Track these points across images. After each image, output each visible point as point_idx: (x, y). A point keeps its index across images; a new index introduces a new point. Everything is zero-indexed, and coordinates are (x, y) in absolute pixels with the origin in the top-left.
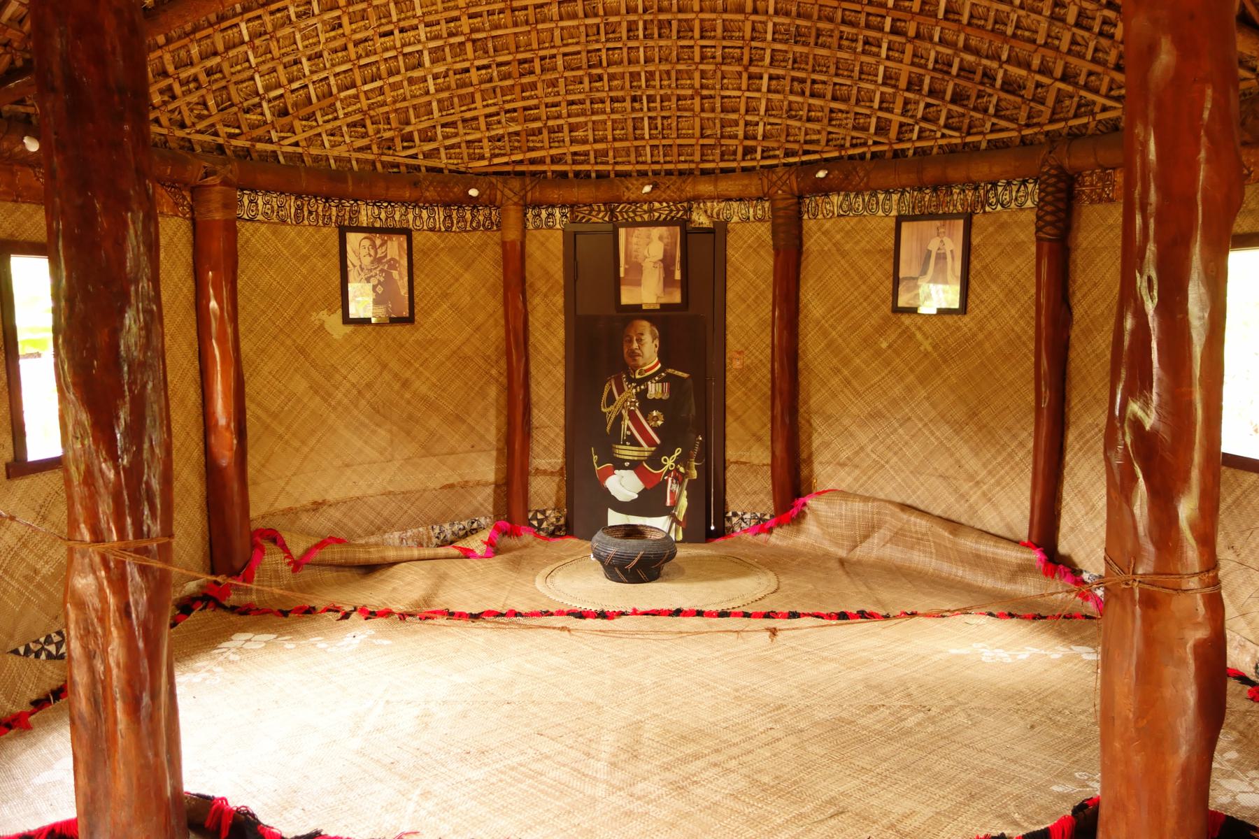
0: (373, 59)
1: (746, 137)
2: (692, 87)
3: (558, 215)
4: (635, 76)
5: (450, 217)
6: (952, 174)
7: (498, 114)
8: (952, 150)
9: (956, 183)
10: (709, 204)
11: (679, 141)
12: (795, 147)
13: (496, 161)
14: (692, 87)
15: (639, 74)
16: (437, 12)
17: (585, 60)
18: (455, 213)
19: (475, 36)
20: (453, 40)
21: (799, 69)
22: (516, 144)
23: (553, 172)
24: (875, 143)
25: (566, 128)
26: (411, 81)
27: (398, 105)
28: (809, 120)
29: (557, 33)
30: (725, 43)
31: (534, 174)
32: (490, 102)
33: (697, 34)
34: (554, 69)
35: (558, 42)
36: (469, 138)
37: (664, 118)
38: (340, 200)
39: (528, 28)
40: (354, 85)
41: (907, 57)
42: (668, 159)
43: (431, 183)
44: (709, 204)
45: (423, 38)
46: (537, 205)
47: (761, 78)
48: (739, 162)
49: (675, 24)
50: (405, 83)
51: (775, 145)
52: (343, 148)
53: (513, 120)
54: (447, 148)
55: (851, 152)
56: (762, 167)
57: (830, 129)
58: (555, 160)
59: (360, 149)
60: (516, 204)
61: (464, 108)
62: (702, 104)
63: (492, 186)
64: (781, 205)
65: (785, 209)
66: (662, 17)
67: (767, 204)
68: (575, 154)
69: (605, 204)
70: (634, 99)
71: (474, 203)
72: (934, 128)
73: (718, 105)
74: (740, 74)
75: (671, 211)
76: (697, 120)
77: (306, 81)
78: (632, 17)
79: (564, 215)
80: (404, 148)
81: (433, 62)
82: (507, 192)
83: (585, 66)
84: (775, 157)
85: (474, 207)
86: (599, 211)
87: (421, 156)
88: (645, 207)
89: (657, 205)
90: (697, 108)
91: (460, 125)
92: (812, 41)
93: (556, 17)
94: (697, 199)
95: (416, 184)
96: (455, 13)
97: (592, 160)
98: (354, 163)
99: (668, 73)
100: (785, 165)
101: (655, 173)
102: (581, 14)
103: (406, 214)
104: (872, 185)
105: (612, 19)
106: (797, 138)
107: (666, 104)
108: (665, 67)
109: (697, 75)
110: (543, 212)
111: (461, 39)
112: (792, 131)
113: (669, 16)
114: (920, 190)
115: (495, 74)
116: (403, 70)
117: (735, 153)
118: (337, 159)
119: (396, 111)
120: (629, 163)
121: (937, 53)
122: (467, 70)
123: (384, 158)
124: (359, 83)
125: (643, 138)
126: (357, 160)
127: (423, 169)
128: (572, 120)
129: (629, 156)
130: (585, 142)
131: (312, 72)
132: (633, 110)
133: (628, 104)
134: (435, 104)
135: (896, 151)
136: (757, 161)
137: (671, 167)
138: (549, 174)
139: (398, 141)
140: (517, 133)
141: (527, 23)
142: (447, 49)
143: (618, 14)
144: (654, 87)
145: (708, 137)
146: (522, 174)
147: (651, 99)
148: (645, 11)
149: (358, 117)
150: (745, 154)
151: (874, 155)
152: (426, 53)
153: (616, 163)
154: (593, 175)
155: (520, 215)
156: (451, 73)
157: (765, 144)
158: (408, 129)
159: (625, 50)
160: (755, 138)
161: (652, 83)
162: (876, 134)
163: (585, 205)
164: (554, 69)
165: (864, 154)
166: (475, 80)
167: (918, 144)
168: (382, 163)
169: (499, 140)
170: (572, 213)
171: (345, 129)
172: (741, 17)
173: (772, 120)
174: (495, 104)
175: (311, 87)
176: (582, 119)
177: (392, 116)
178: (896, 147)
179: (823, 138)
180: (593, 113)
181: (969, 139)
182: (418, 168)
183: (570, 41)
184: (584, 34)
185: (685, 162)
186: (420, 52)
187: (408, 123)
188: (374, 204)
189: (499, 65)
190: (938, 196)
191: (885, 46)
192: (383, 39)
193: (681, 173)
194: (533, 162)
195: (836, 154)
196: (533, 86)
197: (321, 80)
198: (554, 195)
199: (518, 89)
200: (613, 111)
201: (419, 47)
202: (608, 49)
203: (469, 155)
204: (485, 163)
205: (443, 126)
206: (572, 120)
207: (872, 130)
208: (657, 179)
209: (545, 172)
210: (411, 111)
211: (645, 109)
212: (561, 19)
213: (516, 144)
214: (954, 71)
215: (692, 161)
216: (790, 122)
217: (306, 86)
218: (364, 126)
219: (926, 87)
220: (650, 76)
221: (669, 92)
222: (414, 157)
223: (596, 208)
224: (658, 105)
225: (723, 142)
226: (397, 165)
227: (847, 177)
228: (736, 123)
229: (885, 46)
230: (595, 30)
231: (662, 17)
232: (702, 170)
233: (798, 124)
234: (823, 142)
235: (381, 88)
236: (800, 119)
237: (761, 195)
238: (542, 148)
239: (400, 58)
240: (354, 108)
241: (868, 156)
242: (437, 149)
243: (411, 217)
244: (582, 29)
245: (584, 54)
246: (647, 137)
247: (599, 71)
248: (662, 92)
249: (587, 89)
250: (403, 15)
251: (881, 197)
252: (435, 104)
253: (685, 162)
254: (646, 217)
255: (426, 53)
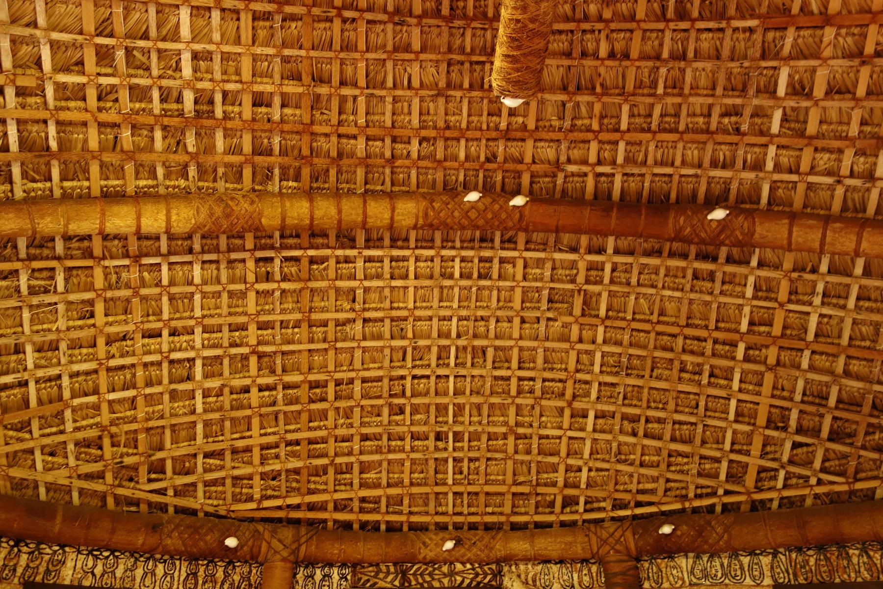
0: (128, 361)
1: (566, 485)
2: (506, 423)
3: (336, 577)
4: (441, 409)
5: (195, 575)
6: (849, 528)
7: (277, 446)
8: (834, 499)
9: (853, 540)
10: (522, 567)
11: (487, 488)
12: (627, 497)
13: (266, 504)
14: (506, 423)
15: (446, 408)
16: (220, 315)
17: (386, 388)
18: (202, 569)
19: (261, 349)
20: (234, 351)
21: (630, 405)
22: (294, 485)
23: (335, 521)
24: (727, 493)
25: (356, 468)
26: (174, 395)
27: (151, 424)
28: (642, 465)
29: (358, 354)
30: (547, 375)
31: (311, 523)
32: (269, 430)
33: (515, 364)
34: (350, 397)
35: (357, 364)
36: (236, 472)
37: (471, 460)
38: (38, 544)
39: (325, 346)
40: (96, 392)
41: (767, 389)
42: (473, 510)
43: (177, 527)
44: (522, 567)
45: (198, 344)
46: (311, 563)
47: (585, 416)
48: (558, 515)
49: (490, 353)
50: (166, 397)
51: (601, 494)
52: (64, 472)
53: (294, 455)
54: (207, 484)
55: (697, 503)
56: (584, 521)
57: (670, 476)
58: (339, 506)
59: (89, 477)
60: (284, 560)
61: (235, 436)
62: (516, 445)
63: (257, 536)
64: (616, 568)
65: (623, 573)
66: (478, 343)
67: (594, 568)
68: (363, 500)
69: (395, 564)
70: (438, 437)
71: (230, 557)
72: (808, 473)
73: (535, 446)
74: (561, 411)
75: (477, 575)
76: (510, 463)
77: (26, 376)
78: (444, 342)
79: (343, 577)
80: (150, 481)
81: (206, 376)
82: (275, 543)
83: (386, 395)
84: (599, 509)
85: (230, 563)
86: (388, 573)
87: (171, 492)
88: (445, 569)
89: (459, 567)
90: (511, 449)
91: (228, 455)
92: (647, 374)
93: (359, 336)
94: (509, 559)
95: (155, 528)
96: (242, 319)
97: (383, 508)
98: (75, 495)
99: (479, 407)
100: (613, 519)
101: (458, 527)
102: (387, 335)
103: (134, 567)
104: (736, 543)
105: (422, 343)
106: (629, 487)
107: (473, 444)
108: (476, 399)
109: (512, 411)
110: (318, 571)
111: (245, 350)
112: (621, 479)
113: (484, 343)
114: (799, 550)
115: (280, 396)
116: (166, 381)
117: (552, 504)
118: (49, 487)
119: (148, 430)
120: (427, 513)
121: (807, 381)
122: (246, 390)
123: (120, 491)
124: (103, 388)
125: (445, 484)
126: (81, 491)
127: (171, 510)
128: (364, 458)
129: (426, 505)
130: (377, 485)
131: (37, 366)
132: (437, 449)
133: (431, 443)
134: (200, 427)
135: (753, 502)
136: (579, 513)
137: (476, 519)
138: (330, 524)
139: (143, 470)
140: (297, 471)
141: (325, 340)
142: (226, 362)
143: (429, 337)
144: (462, 423)
145: (520, 484)
146: (297, 522)
147: (458, 437)
148: (459, 336)
149: (93, 433)
150: (564, 507)
151: (725, 507)
152: (199, 363)
153: (411, 513)
154: (383, 527)
155: (288, 574)
156: (226, 391)
157: (590, 493)
158: (160, 455)
159: (433, 378)
160: (576, 486)
161: (460, 419)
162: (727, 481)
163: (371, 565)
164: (350, 397)
165: (713, 506)
166: (255, 402)
167: (786, 493)
168: (116, 497)
169: (274, 479)
170: (354, 574)
171: (71, 447)
172: (566, 345)
173: (599, 465)
174: (274, 433)
175: (32, 385)
176: (376, 457)
177: (141, 436)
178: (757, 497)
179: (661, 485)
180: (389, 451)
181: (859, 486)
182: (164, 508)
183: (372, 365)
184: (388, 359)
185: (493, 513)
186: (192, 361)
187: (161, 449)
188: (90, 553)
189: (286, 387)
190: (827, 559)
191: (737, 377)
192: (146, 340)
193: (488, 527)
194: (311, 507)
195: (677, 506)
196: (324, 415)
197: (50, 379)
198: (334, 549)
199: (305, 416)
200: (413, 450)
201: (191, 354)
202: (414, 377)
203: (234, 495)
204: (253, 505)
205: (207, 456)
206: (364, 458)
207: (723, 477)
208: (458, 533)
209: (325, 521)
210: (168, 432)
211: (451, 448)
212: (365, 339)
213: (294, 485)
214: (832, 402)
215: (501, 514)
216: (620, 467)
217: (26, 384)
218: (101, 448)
219: (793, 423)
220: (459, 408)
221: (480, 429)
222: (162, 492)
223: (384, 568)
224: (465, 444)
225: (540, 490)
226: (137, 503)
227: (700, 533)
228: (554, 469)
229: (737, 377)
230: (401, 354)
231: (478, 343)
232: (512, 523)
233: (630, 469)
234: (660, 492)
235: (134, 399)
236: (632, 464)
237: (588, 556)
238: (325, 491)
239: (165, 365)
240: (91, 421)
241: (719, 509)
242: (194, 485)
243: (139, 572)
244: (387, 352)
245: (386, 381)
246: (450, 482)
247: (401, 401)
248: (472, 429)
249: (386, 422)
250: (178, 315)
251: (746, 560)
252: (200, 427)
253: (493, 513)
254: (446, 581)
255: (199, 363)
